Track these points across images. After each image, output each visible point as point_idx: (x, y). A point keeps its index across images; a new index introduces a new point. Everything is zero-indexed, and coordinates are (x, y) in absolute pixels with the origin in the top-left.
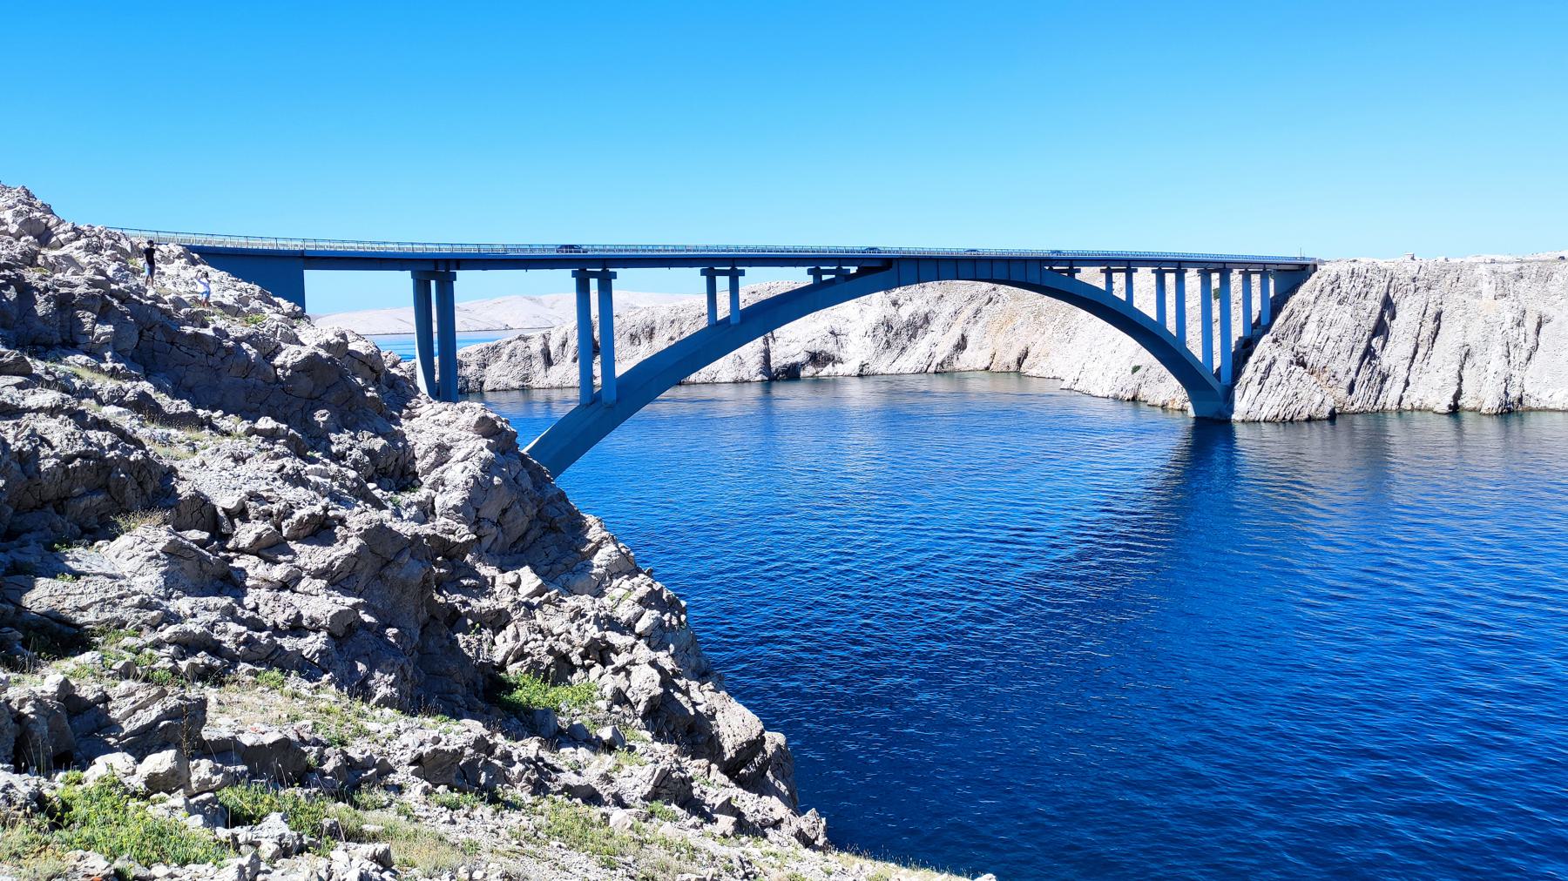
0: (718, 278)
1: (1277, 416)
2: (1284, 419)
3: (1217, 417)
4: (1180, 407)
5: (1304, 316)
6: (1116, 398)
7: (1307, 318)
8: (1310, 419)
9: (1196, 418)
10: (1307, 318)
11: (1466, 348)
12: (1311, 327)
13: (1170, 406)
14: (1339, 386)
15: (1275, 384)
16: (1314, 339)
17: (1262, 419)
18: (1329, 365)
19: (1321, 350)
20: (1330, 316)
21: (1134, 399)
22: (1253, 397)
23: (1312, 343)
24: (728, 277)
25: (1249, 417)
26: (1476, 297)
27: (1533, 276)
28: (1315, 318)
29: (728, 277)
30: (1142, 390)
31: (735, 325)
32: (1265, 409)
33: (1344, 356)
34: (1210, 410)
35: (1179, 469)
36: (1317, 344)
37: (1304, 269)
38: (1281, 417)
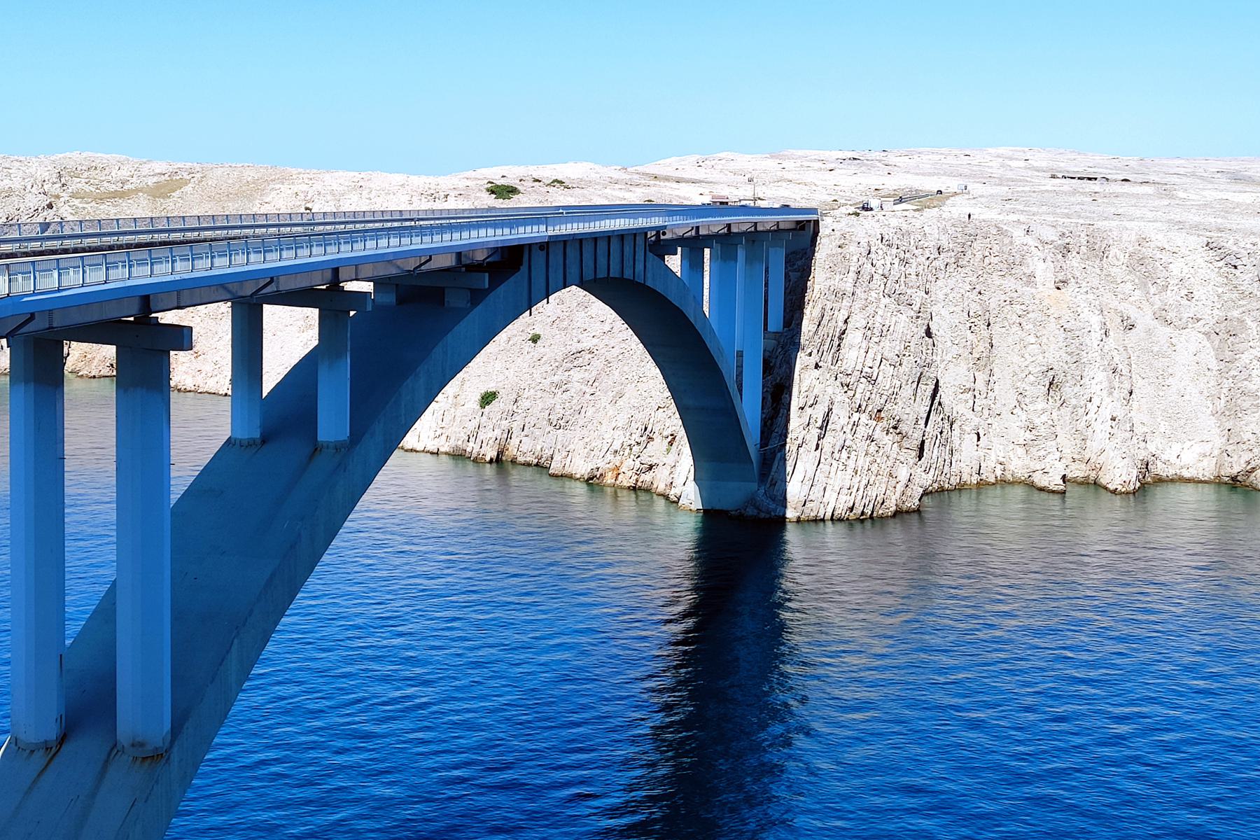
0: (273, 315)
1: (851, 509)
2: (863, 513)
3: (751, 511)
4: (632, 483)
5: (841, 318)
6: (458, 456)
7: (846, 322)
8: (898, 513)
9: (711, 517)
10: (846, 322)
11: (1051, 373)
12: (854, 338)
13: (609, 479)
14: (905, 444)
15: (838, 448)
16: (861, 360)
17: (828, 516)
18: (888, 406)
19: (872, 380)
20: (878, 318)
21: (498, 461)
22: (810, 474)
23: (859, 367)
24: (313, 313)
25: (807, 511)
26: (1028, 283)
27: (1084, 249)
28: (858, 321)
29: (313, 313)
30: (514, 442)
31: (338, 447)
32: (831, 497)
33: (908, 391)
34: (734, 495)
35: (786, 632)
36: (866, 369)
37: (803, 228)
38: (858, 510)
